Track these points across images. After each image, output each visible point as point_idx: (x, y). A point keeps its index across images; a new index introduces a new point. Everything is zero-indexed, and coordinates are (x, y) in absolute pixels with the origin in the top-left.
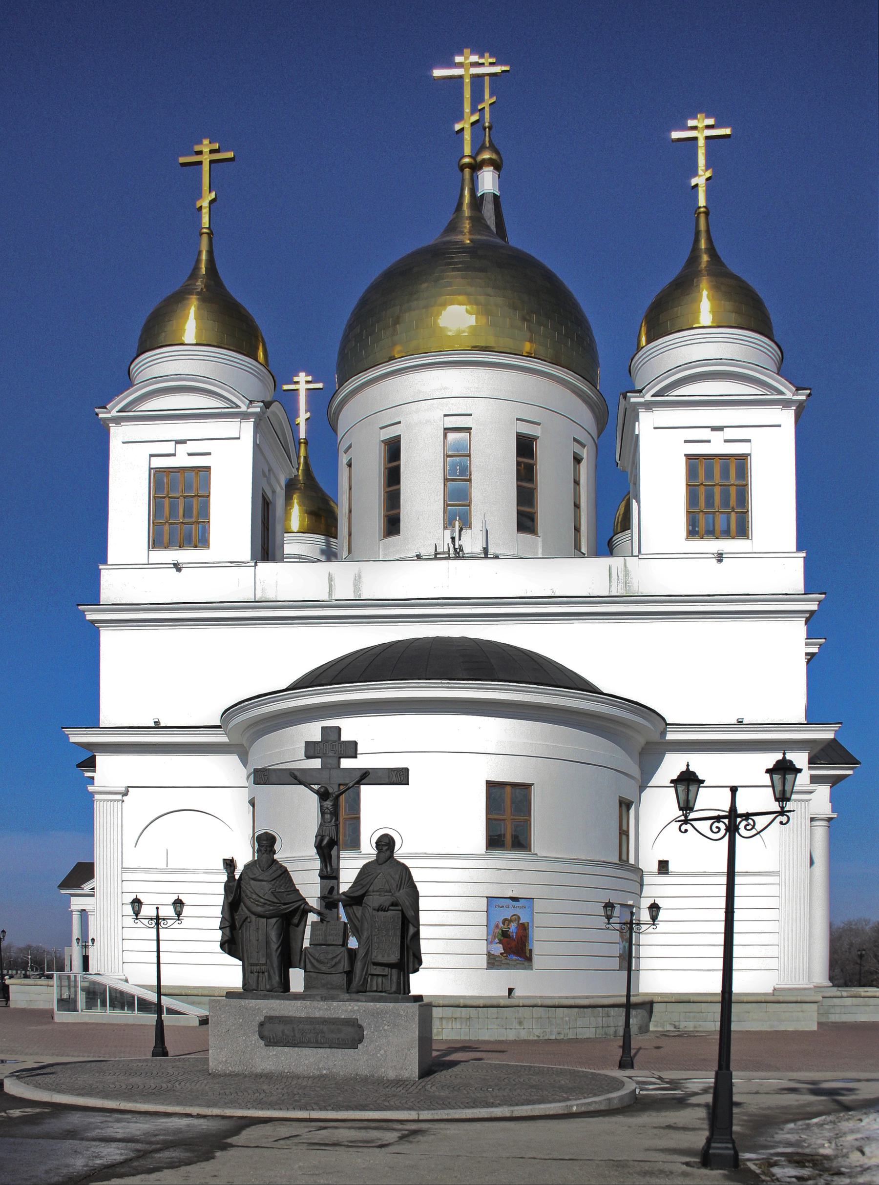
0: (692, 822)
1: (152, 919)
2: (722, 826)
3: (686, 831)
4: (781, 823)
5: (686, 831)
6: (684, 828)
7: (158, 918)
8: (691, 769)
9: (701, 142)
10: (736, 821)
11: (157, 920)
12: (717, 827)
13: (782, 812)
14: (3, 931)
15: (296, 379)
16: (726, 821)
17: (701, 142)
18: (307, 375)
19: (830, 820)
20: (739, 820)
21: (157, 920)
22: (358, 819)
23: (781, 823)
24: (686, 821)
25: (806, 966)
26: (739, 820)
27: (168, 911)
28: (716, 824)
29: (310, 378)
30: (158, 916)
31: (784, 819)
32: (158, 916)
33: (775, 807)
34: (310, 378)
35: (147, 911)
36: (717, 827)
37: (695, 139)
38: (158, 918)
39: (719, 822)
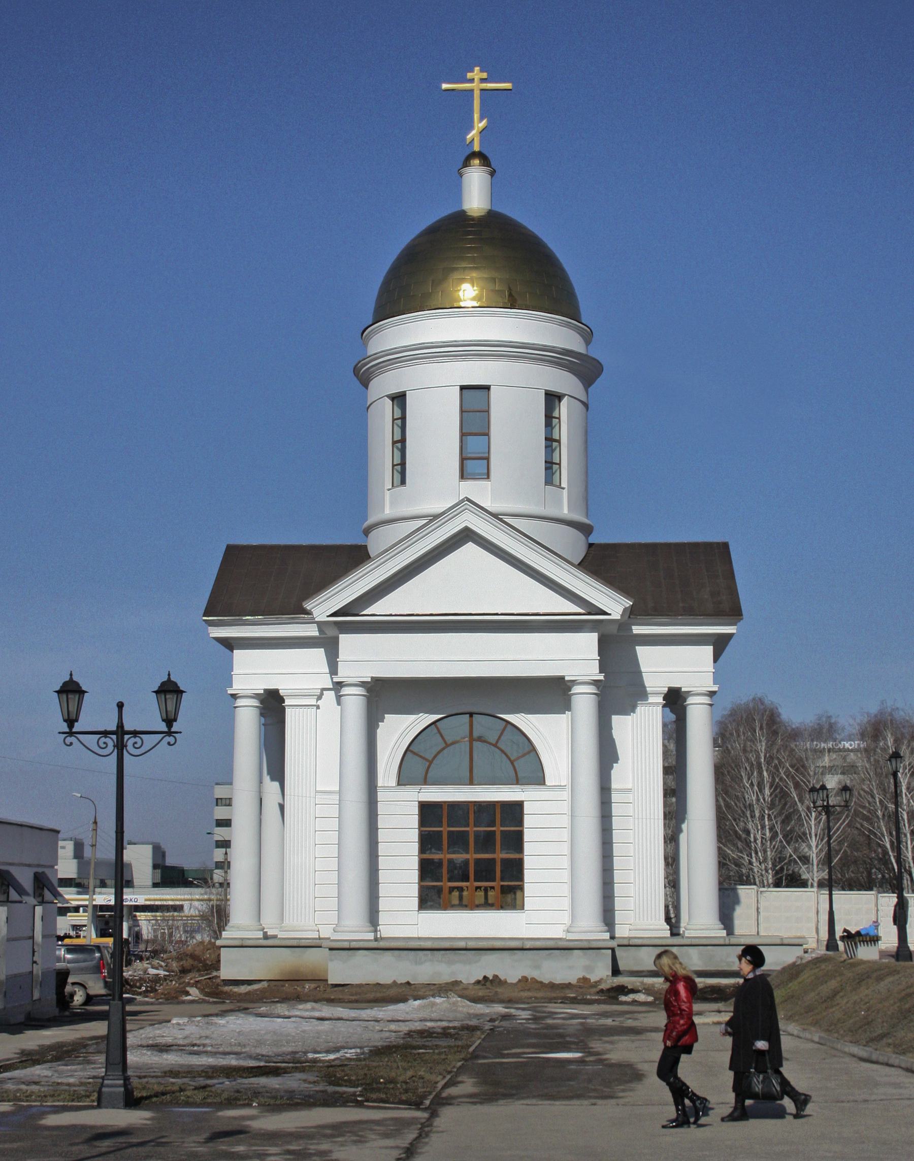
0: (79, 736)
1: (105, 733)
2: (111, 744)
3: (71, 744)
4: (169, 744)
5: (71, 744)
6: (69, 740)
7: (120, 731)
8: (75, 679)
9: (477, 94)
10: (123, 739)
11: (120, 735)
12: (105, 743)
13: (169, 733)
14: (169, 690)
15: (469, 75)
16: (114, 737)
17: (477, 94)
18: (482, 71)
19: (712, 694)
20: (126, 737)
21: (120, 735)
22: (696, 545)
23: (169, 744)
24: (71, 733)
25: (305, 928)
26: (126, 737)
27: (145, 714)
28: (103, 740)
29: (485, 75)
30: (120, 725)
31: (171, 739)
32: (120, 725)
33: (163, 727)
34: (485, 75)
35: (96, 714)
36: (105, 743)
37: (472, 91)
38: (120, 731)
39: (135, 737)
